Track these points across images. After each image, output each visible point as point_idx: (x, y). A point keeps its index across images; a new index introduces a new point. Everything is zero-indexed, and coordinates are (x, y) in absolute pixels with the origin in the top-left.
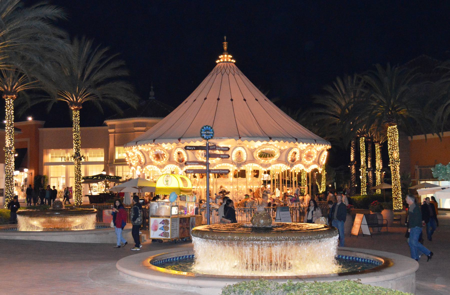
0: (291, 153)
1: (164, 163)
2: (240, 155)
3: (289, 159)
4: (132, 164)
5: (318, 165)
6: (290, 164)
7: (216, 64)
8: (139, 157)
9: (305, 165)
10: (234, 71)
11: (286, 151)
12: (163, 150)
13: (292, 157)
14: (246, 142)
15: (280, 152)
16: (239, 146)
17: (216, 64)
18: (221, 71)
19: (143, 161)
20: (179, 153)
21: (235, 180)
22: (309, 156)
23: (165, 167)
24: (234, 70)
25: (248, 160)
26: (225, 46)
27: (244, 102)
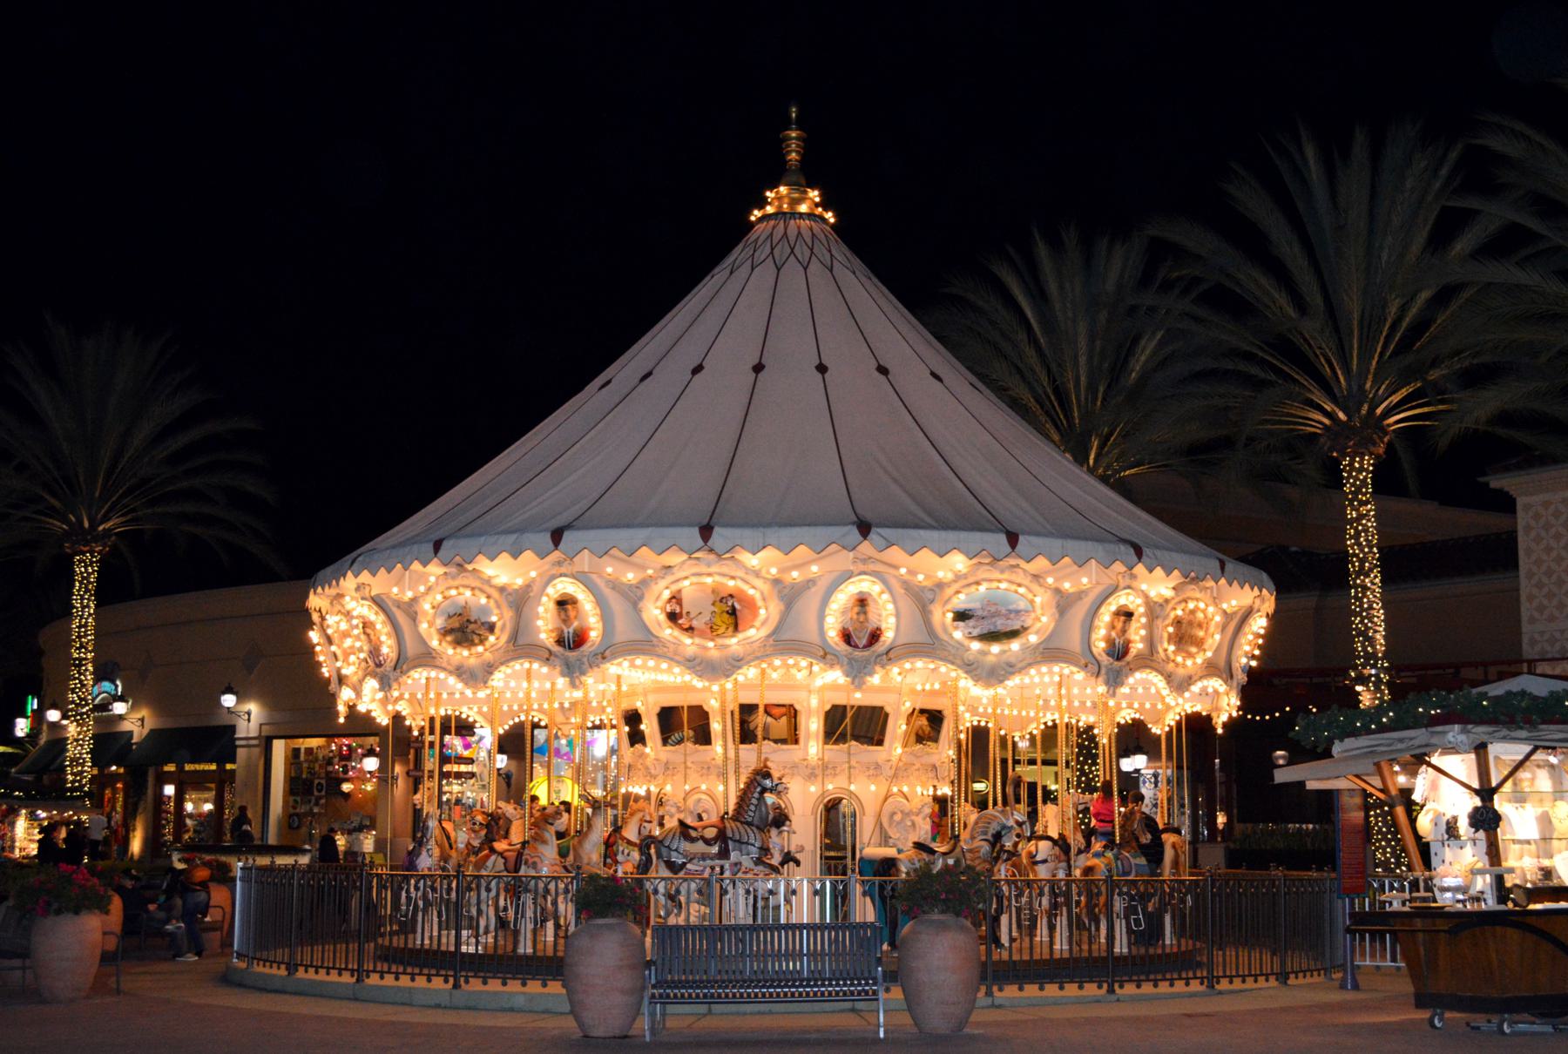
0: (1105, 616)
1: (488, 656)
2: (865, 613)
4: (344, 672)
5: (1226, 682)
6: (1103, 671)
7: (751, 225)
8: (368, 631)
9: (1169, 678)
10: (832, 255)
11: (1087, 601)
12: (482, 590)
13: (1114, 634)
14: (895, 554)
15: (1058, 606)
16: (861, 567)
17: (751, 225)
18: (772, 253)
19: (388, 649)
20: (563, 603)
21: (836, 752)
22: (1185, 636)
23: (491, 673)
24: (830, 251)
25: (901, 641)
26: (789, 146)
27: (882, 378)
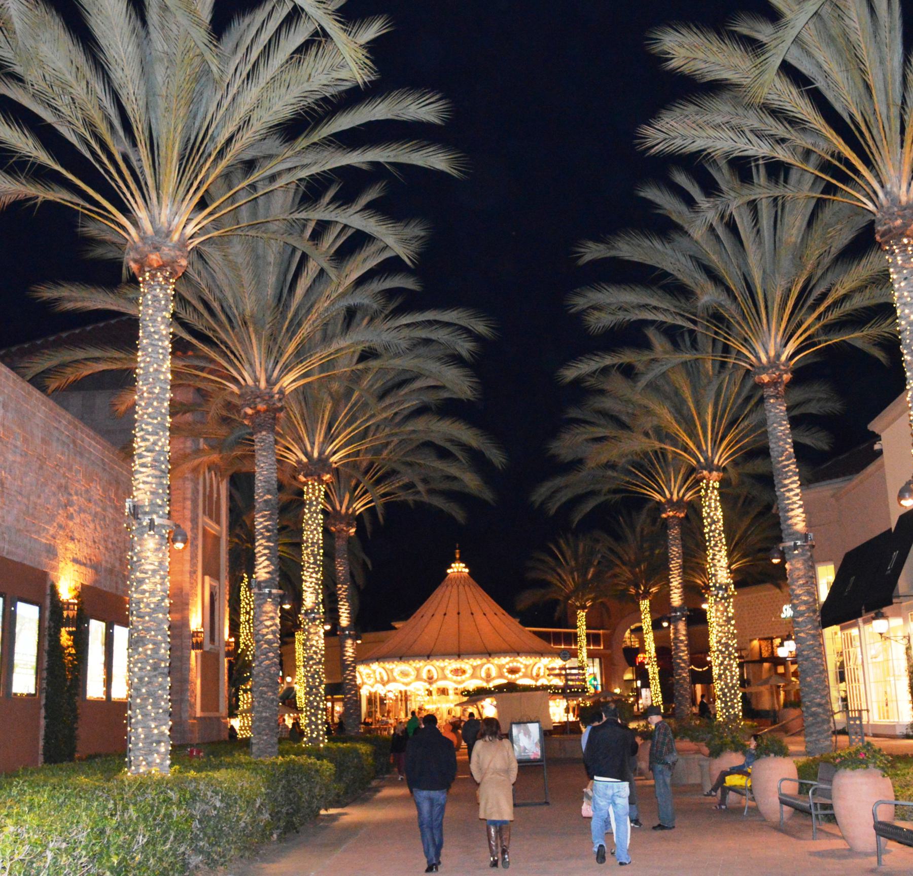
3: (534, 674)
17: (447, 574)
19: (386, 678)
